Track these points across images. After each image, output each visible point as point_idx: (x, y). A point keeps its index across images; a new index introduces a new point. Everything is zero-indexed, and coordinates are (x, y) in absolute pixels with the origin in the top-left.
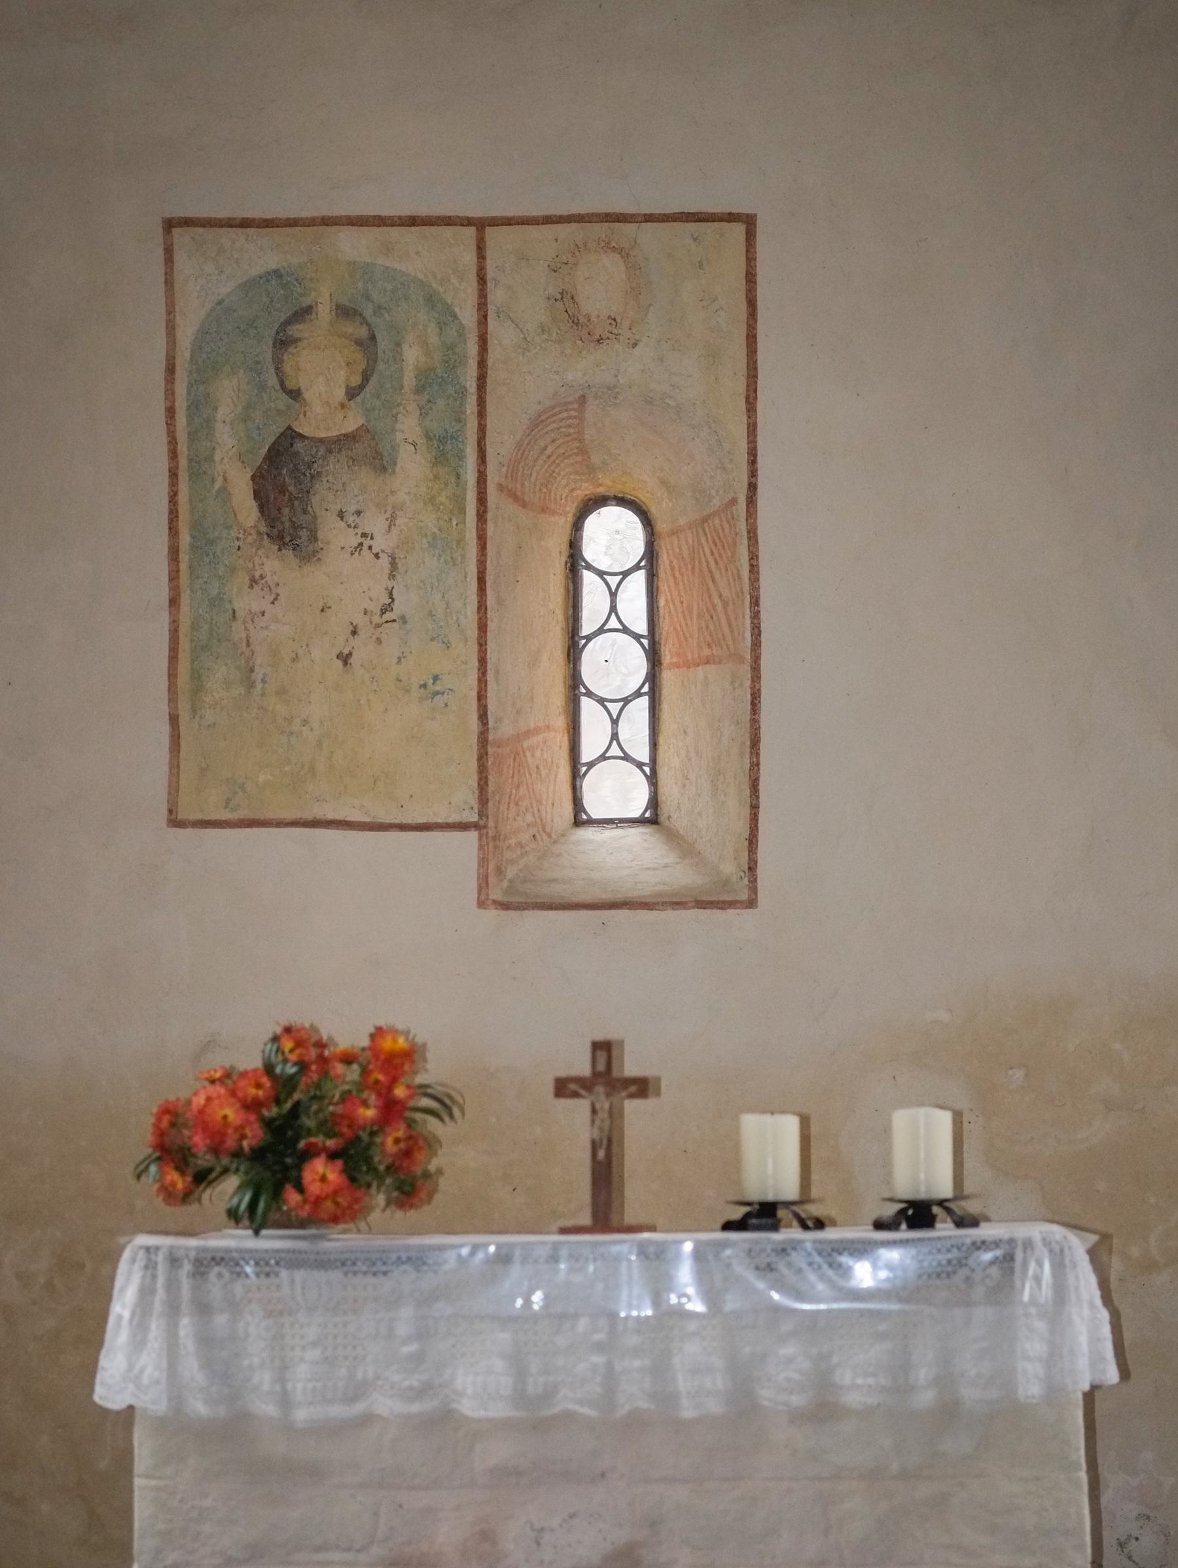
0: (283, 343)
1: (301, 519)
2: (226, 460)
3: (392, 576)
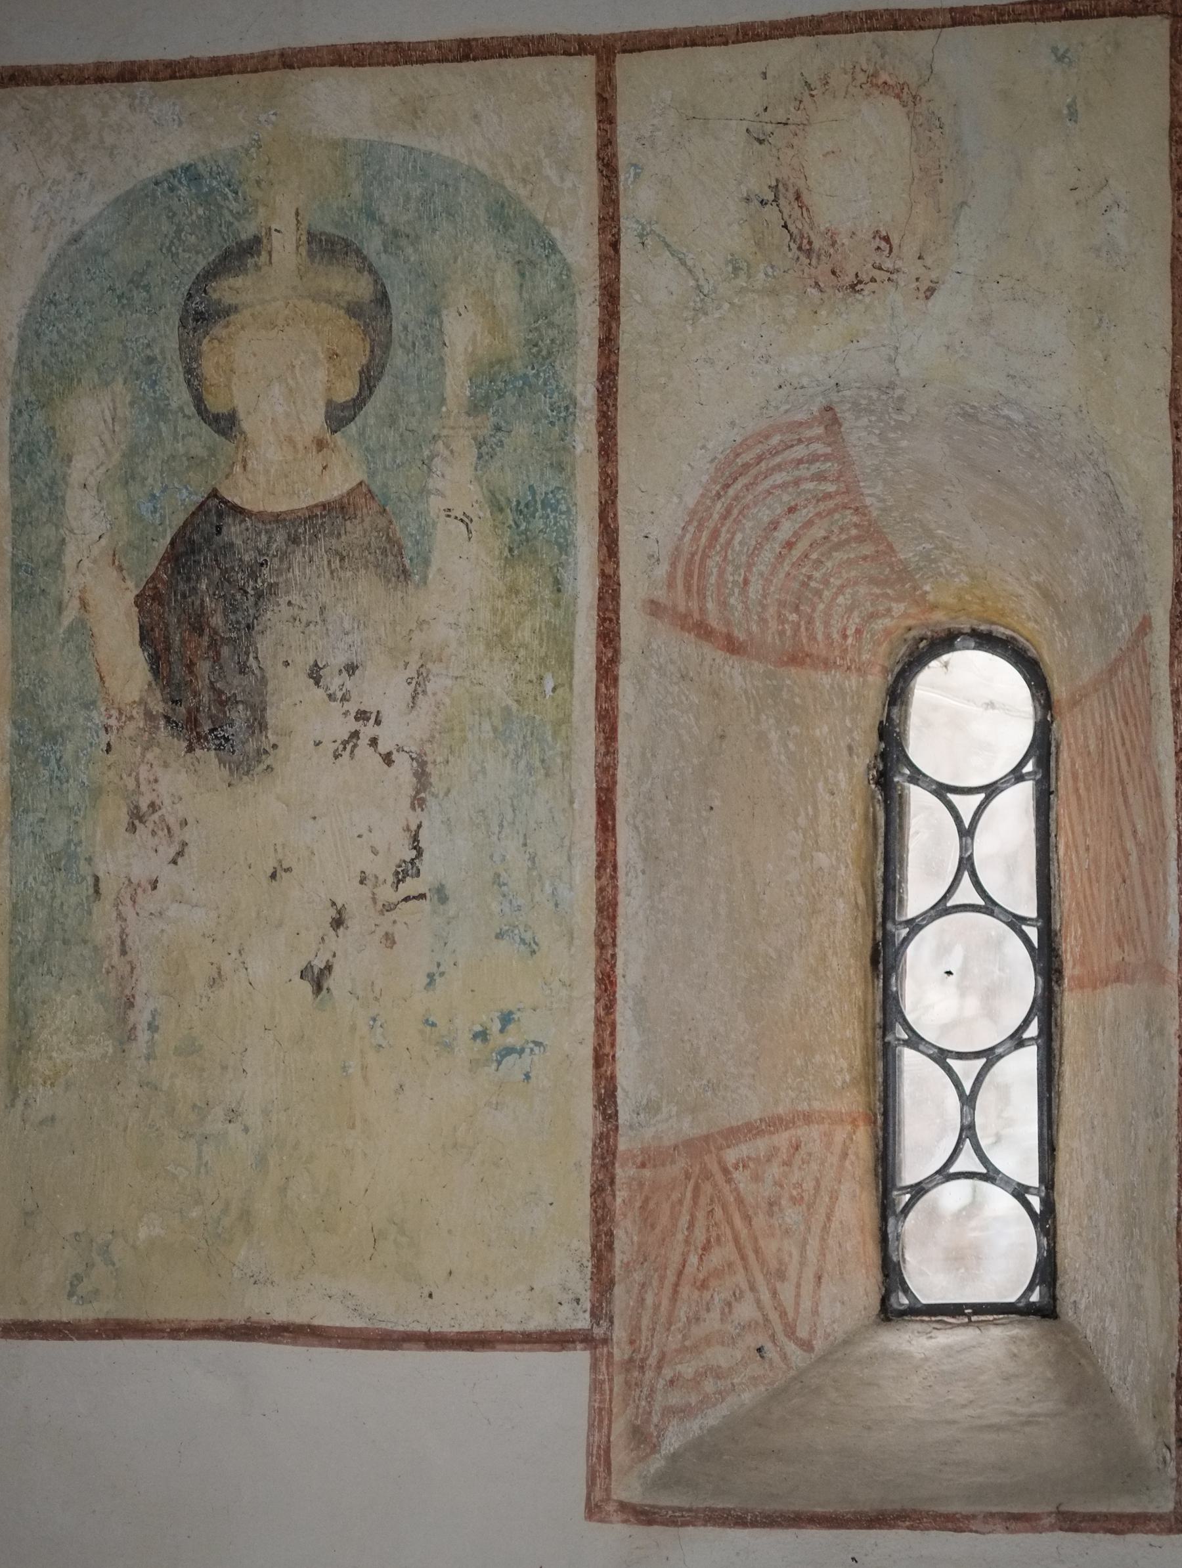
0: (201, 317)
1: (236, 684)
2: (86, 563)
3: (418, 802)
